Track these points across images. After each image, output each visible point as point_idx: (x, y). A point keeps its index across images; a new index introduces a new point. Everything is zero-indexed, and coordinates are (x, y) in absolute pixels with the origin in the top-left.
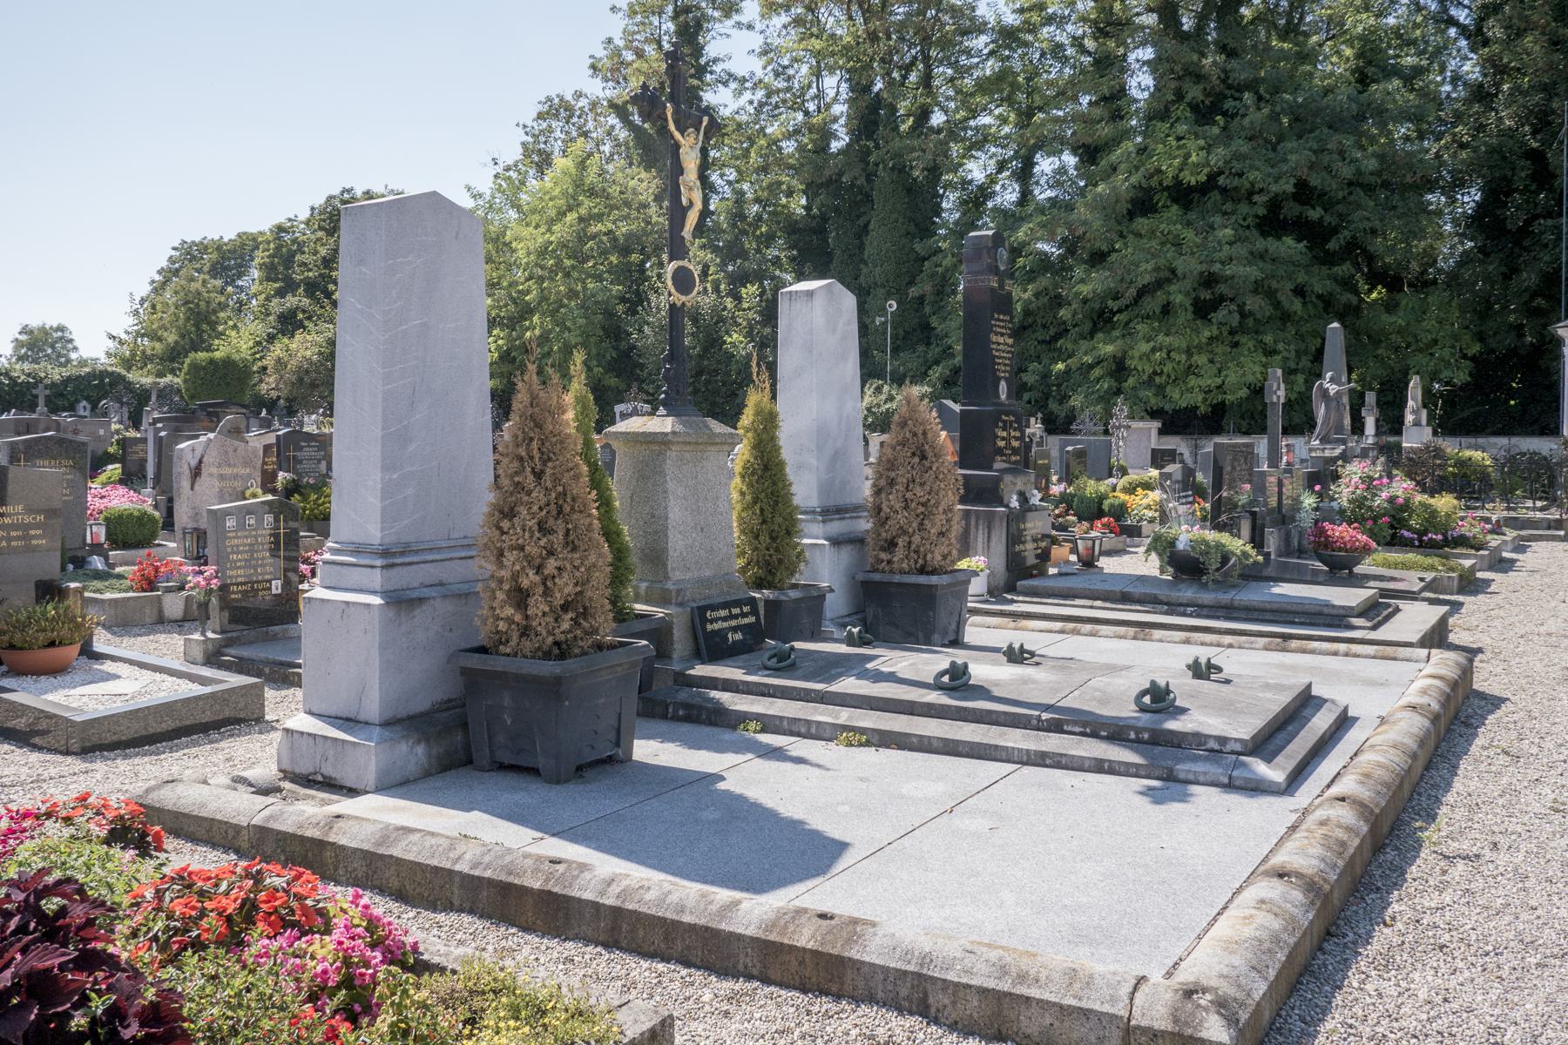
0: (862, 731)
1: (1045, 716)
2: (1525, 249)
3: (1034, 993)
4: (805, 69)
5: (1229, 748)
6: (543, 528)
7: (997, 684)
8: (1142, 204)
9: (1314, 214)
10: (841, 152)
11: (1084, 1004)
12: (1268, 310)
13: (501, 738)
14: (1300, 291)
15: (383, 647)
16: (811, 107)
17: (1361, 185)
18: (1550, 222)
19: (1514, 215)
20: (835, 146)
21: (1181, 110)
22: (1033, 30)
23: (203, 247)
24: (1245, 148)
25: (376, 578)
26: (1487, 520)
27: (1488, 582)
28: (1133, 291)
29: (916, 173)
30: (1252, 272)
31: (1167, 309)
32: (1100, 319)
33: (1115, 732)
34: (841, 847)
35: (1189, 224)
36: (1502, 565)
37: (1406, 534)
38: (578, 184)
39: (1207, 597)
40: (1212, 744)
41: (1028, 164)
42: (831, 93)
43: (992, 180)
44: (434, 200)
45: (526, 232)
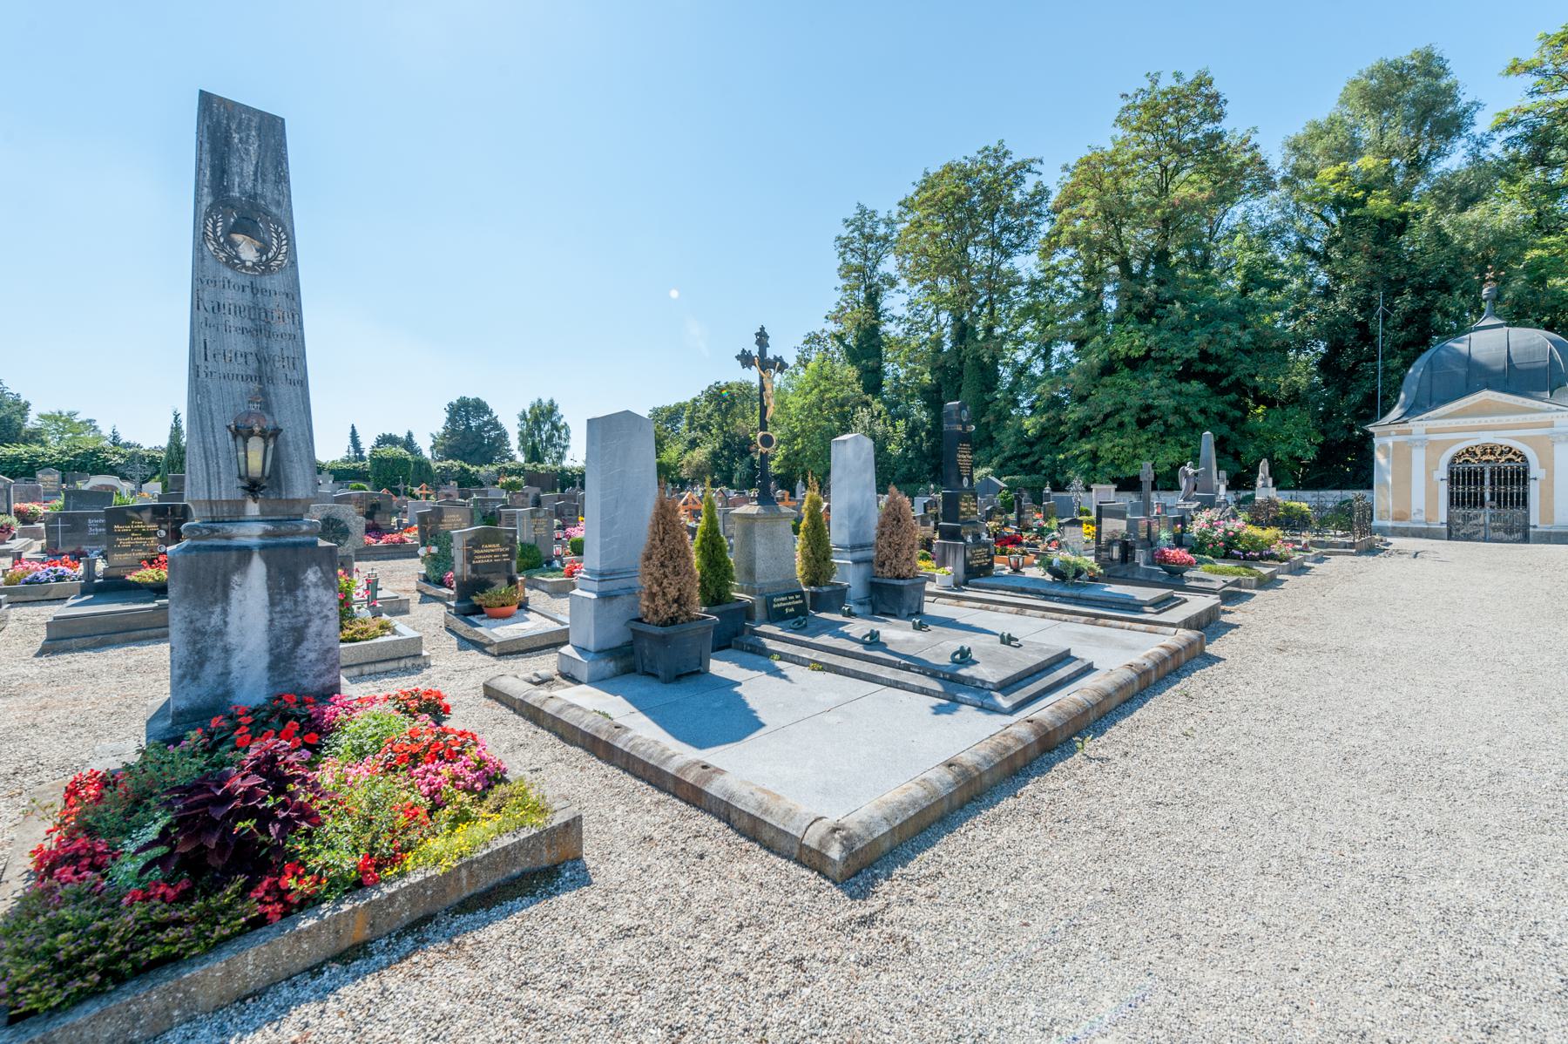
0: (821, 663)
1: (903, 662)
2: (1355, 380)
3: (768, 819)
4: (930, 311)
5: (986, 686)
6: (663, 565)
7: (893, 642)
8: (1108, 369)
9: (1212, 368)
10: (949, 351)
11: (786, 829)
12: (1183, 423)
13: (646, 661)
14: (1203, 411)
15: (596, 618)
16: (934, 329)
17: (1242, 351)
18: (1370, 364)
19: (1346, 360)
20: (946, 348)
21: (1131, 317)
22: (1048, 279)
23: (663, 410)
24: (1168, 335)
25: (596, 586)
26: (1299, 542)
27: (1282, 581)
28: (1101, 416)
29: (986, 360)
30: (1172, 403)
31: (1121, 425)
32: (1084, 432)
33: (932, 672)
34: (762, 725)
35: (1135, 378)
36: (1300, 570)
37: (1236, 552)
38: (821, 377)
39: (1066, 592)
40: (979, 684)
41: (1049, 351)
42: (943, 322)
43: (1029, 360)
44: (628, 415)
45: (794, 399)
